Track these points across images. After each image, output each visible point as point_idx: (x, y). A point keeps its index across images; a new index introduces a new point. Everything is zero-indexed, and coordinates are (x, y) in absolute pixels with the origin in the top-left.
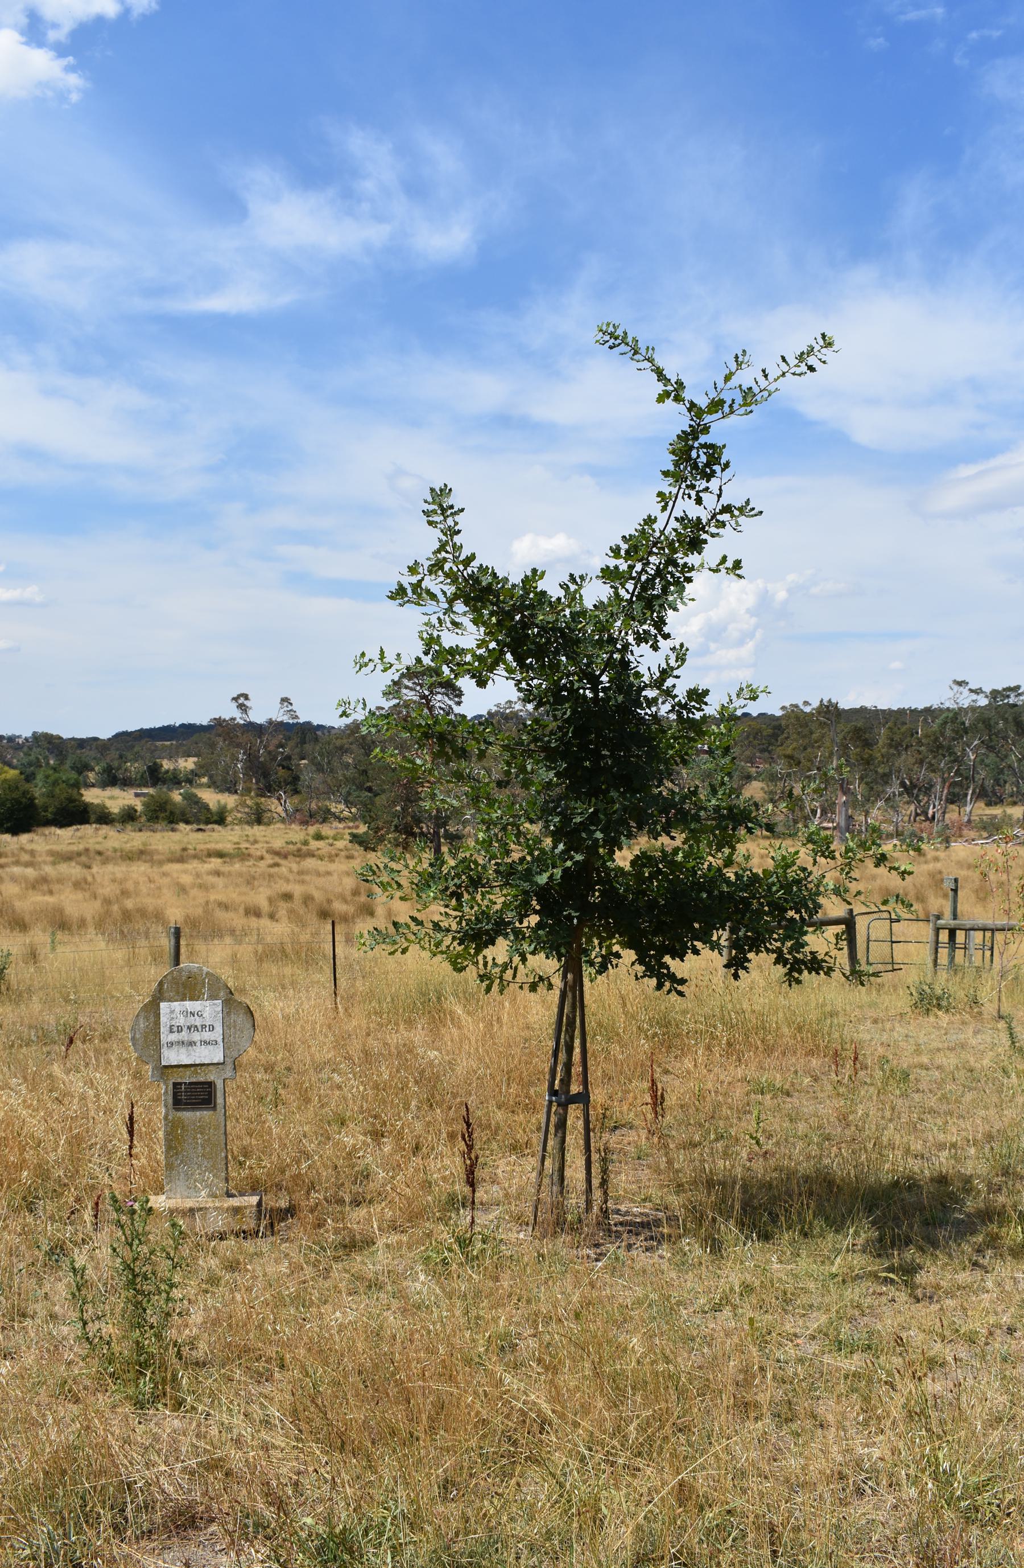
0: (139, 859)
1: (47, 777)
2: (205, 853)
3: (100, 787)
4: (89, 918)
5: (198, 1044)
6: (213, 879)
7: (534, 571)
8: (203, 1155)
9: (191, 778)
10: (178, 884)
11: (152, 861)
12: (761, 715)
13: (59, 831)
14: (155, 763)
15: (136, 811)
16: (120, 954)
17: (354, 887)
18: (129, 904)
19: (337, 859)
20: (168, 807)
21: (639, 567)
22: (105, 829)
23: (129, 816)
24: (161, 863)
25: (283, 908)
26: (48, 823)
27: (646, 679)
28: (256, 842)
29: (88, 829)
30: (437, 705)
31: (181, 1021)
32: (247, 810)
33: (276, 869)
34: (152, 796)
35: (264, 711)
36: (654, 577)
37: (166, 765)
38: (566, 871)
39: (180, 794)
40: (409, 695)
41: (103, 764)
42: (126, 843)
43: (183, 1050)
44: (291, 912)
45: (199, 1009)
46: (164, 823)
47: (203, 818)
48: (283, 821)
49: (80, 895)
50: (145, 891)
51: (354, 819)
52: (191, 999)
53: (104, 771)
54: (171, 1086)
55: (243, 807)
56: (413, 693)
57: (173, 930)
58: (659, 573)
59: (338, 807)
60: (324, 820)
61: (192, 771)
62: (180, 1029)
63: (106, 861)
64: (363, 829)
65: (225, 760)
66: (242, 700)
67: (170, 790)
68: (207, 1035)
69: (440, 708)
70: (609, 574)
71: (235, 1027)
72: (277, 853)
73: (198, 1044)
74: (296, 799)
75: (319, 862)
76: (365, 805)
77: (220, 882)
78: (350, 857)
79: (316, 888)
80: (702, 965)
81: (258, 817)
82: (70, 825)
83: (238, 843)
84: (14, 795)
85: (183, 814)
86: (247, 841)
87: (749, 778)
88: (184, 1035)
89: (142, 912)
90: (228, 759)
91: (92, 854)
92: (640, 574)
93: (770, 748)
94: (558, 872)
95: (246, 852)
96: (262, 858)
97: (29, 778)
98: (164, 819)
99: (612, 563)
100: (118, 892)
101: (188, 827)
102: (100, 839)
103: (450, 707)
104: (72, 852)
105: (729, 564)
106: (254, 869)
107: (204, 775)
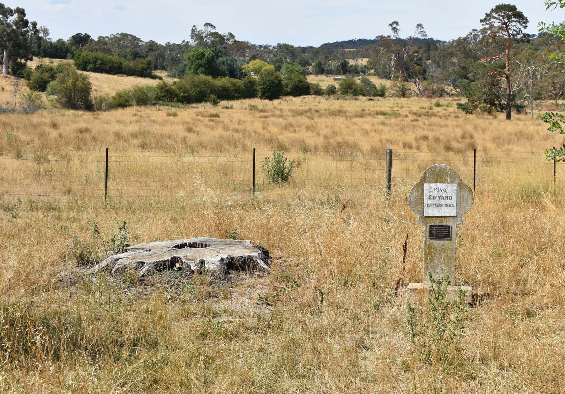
0: (338, 115)
1: (288, 68)
2: (375, 112)
5: (444, 206)
6: (381, 127)
8: (444, 264)
9: (364, 70)
10: (362, 129)
13: (294, 99)
14: (345, 61)
15: (335, 88)
16: (344, 165)
18: (339, 139)
19: (449, 118)
20: (353, 86)
22: (319, 98)
23: (332, 91)
24: (351, 117)
25: (424, 144)
26: (288, 94)
28: (402, 107)
29: (309, 98)
31: (435, 193)
32: (397, 89)
33: (415, 123)
34: (345, 80)
37: (351, 62)
39: (359, 79)
40: (497, 24)
42: (331, 106)
43: (436, 209)
44: (428, 146)
46: (351, 95)
48: (417, 95)
49: (310, 134)
50: (345, 132)
51: (458, 95)
52: (441, 182)
53: (317, 66)
54: (429, 227)
56: (498, 21)
57: (388, 151)
60: (441, 96)
61: (365, 66)
62: (434, 198)
63: (320, 116)
65: (384, 60)
66: (394, 25)
68: (448, 202)
69: (514, 30)
71: (463, 198)
72: (415, 114)
73: (444, 206)
74: (425, 83)
75: (439, 119)
76: (465, 87)
77: (386, 129)
78: (457, 117)
79: (440, 133)
81: (403, 93)
82: (300, 95)
83: (392, 108)
84: (272, 78)
85: (362, 90)
86: (398, 106)
88: (436, 201)
95: (398, 112)
96: (407, 116)
97: (278, 68)
100: (330, 132)
101: (364, 98)
102: (316, 104)
103: (520, 30)
104: (302, 110)
106: (404, 123)
107: (372, 69)
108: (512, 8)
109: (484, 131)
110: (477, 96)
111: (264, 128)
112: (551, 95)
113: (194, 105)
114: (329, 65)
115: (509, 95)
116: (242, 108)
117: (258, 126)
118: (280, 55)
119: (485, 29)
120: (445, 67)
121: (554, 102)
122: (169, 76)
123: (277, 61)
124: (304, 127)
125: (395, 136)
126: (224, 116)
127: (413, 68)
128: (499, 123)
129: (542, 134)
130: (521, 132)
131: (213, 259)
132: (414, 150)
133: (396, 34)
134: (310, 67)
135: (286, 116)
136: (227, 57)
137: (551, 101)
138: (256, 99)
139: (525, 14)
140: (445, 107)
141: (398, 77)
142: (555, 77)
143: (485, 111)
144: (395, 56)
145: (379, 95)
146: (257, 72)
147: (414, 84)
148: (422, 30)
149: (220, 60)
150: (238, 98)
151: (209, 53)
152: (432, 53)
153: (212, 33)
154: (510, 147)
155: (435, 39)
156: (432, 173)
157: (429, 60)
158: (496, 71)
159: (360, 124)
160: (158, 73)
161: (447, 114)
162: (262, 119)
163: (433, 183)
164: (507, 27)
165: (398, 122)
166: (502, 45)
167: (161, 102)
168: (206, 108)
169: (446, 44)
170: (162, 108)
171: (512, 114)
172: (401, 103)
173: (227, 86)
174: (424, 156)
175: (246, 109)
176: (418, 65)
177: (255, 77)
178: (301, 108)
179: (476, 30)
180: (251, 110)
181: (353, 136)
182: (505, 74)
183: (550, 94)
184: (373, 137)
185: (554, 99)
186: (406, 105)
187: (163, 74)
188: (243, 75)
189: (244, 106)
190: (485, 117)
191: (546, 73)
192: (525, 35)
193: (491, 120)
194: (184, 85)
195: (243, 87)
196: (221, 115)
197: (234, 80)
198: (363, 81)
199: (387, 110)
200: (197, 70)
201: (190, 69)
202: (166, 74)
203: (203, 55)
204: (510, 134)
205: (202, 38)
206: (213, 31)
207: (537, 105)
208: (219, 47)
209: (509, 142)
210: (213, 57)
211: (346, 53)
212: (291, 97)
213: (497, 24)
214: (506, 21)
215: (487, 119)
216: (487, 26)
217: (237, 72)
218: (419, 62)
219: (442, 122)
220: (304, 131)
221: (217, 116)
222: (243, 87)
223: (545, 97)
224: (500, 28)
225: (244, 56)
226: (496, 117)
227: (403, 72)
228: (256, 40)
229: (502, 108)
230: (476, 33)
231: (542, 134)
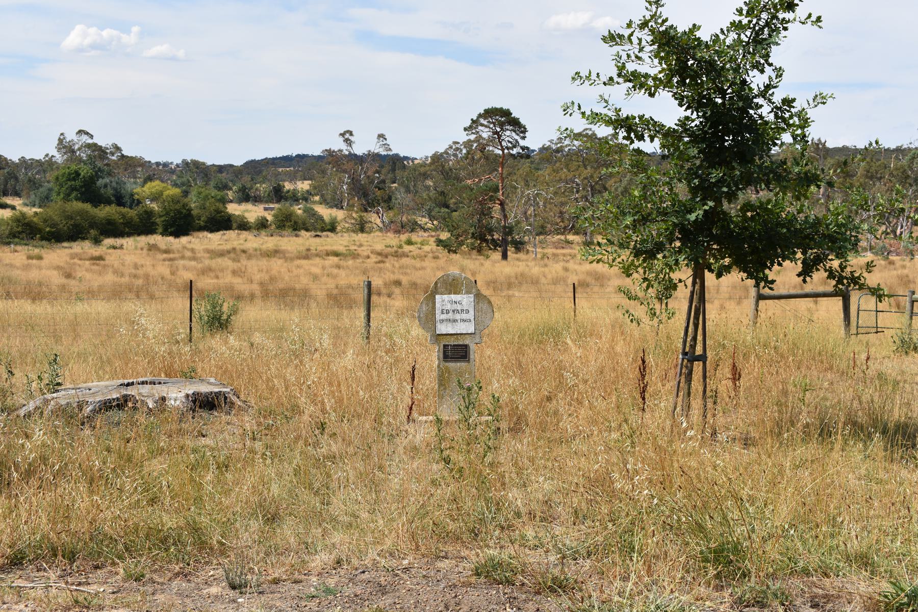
1: (200, 193)
6: (335, 271)
7: (694, 25)
10: (310, 273)
11: (286, 259)
13: (209, 235)
14: (279, 185)
21: (755, 21)
22: (245, 234)
23: (262, 225)
24: (292, 259)
25: (397, 291)
26: (201, 229)
27: (756, 92)
28: (361, 245)
29: (231, 234)
31: (449, 307)
32: (353, 221)
33: (381, 265)
36: (764, 27)
37: (288, 186)
38: (705, 211)
40: (486, 134)
42: (262, 244)
43: (450, 325)
48: (381, 230)
51: (436, 229)
52: (455, 293)
53: (240, 190)
54: (442, 347)
56: (487, 130)
58: (767, 24)
59: (423, 221)
61: (308, 191)
62: (448, 312)
63: (249, 257)
66: (347, 136)
68: (464, 316)
70: (737, 26)
72: (379, 254)
74: (391, 213)
75: (413, 261)
76: (444, 219)
77: (343, 273)
80: (786, 274)
81: (362, 227)
82: (218, 230)
84: (177, 207)
85: (304, 224)
92: (755, 25)
94: (701, 212)
96: (368, 257)
97: (186, 193)
99: (737, 19)
100: (267, 278)
101: (308, 234)
102: (242, 242)
103: (517, 141)
104: (223, 250)
105: (814, 18)
107: (316, 195)
108: (506, 113)
111: (173, 273)
113: (65, 244)
115: (505, 227)
116: (136, 248)
117: (163, 269)
118: (187, 177)
119: (469, 141)
120: (417, 192)
121: (563, 237)
122: (26, 205)
123: (183, 184)
124: (229, 272)
126: (112, 258)
128: (491, 267)
129: (549, 276)
130: (522, 275)
131: (177, 394)
133: (349, 148)
134: (230, 193)
135: (200, 258)
136: (110, 178)
137: (559, 237)
138: (155, 236)
139: (522, 121)
140: (419, 246)
141: (353, 206)
143: (473, 249)
144: (349, 178)
145: (329, 230)
146: (155, 198)
148: (385, 142)
149: (100, 182)
150: (129, 235)
151: (85, 171)
152: (399, 173)
153: (89, 144)
154: (511, 292)
155: (402, 156)
159: (307, 268)
160: (9, 200)
161: (423, 254)
162: (167, 263)
164: (499, 138)
166: (493, 163)
167: (17, 240)
168: (84, 247)
169: (416, 162)
170: (19, 248)
171: (509, 253)
173: (113, 217)
175: (142, 249)
176: (379, 189)
177: (155, 206)
178: (221, 247)
180: (149, 250)
182: (499, 200)
185: (562, 234)
187: (17, 202)
188: (135, 202)
189: (139, 246)
191: (551, 198)
192: (523, 148)
194: (50, 217)
195: (136, 219)
196: (107, 257)
197: (125, 210)
198: (306, 210)
199: (341, 249)
200: (69, 195)
201: (59, 194)
202: (21, 202)
203: (77, 174)
205: (73, 152)
206: (90, 141)
207: (540, 242)
208: (99, 164)
210: (91, 178)
211: (279, 174)
212: (205, 233)
213: (486, 134)
214: (498, 129)
216: (473, 137)
217: (127, 199)
218: (381, 186)
219: (418, 264)
220: (230, 276)
221: (100, 258)
222: (136, 219)
224: (490, 141)
225: (135, 178)
228: (152, 157)
229: (495, 244)
231: (549, 276)
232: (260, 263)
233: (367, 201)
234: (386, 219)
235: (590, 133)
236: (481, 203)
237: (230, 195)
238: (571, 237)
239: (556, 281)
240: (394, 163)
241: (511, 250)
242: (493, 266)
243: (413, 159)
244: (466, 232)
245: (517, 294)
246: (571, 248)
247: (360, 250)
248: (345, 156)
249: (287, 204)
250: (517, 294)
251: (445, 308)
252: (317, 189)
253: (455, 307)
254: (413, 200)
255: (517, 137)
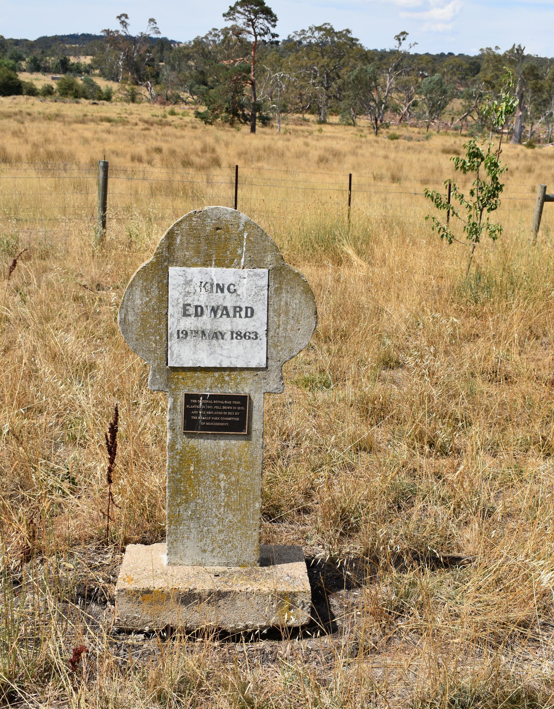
2: (99, 118)
3: (29, 72)
4: (23, 155)
5: (228, 336)
6: (105, 136)
8: (227, 505)
9: (88, 70)
10: (83, 137)
11: (64, 122)
12: (461, 55)
14: (65, 58)
15: (53, 88)
16: (48, 182)
17: (202, 146)
18: (52, 148)
19: (186, 129)
20: (74, 87)
22: (33, 99)
23: (48, 92)
24: (70, 123)
25: (157, 158)
28: (131, 114)
29: (21, 99)
30: (259, 26)
31: (202, 298)
32: (125, 92)
33: (146, 132)
34: (64, 79)
35: (135, 29)
37: (73, 60)
39: (82, 80)
41: (32, 57)
43: (203, 344)
44: (162, 160)
45: (231, 280)
46: (72, 97)
47: (96, 96)
48: (149, 101)
49: (16, 140)
51: (195, 103)
52: (220, 264)
53: (32, 61)
54: (181, 399)
55: (123, 90)
56: (243, 17)
57: (102, 164)
59: (185, 95)
60: (176, 103)
61: (89, 65)
62: (199, 312)
63: (33, 120)
64: (203, 109)
67: (75, 76)
68: (242, 324)
69: (261, 29)
71: (287, 313)
72: (146, 122)
73: (228, 336)
74: (158, 87)
75: (175, 130)
76: (203, 95)
77: (111, 137)
78: (194, 128)
79: (177, 144)
81: (133, 98)
82: (9, 94)
83: (120, 114)
85: (84, 92)
87: (453, 96)
88: (206, 322)
89: (61, 154)
90: (113, 58)
91: (24, 115)
93: (466, 77)
95: (126, 119)
96: (136, 124)
98: (71, 95)
100: (42, 140)
101: (87, 101)
102: (29, 106)
103: (268, 29)
104: (11, 113)
106: (133, 131)
107: (97, 68)
109: (227, 145)
110: (218, 104)
112: (297, 108)
114: (46, 61)
115: (254, 104)
119: (226, 28)
121: (301, 116)
125: (121, 147)
127: (144, 70)
128: (242, 138)
129: (293, 150)
132: (145, 165)
133: (125, 29)
137: (298, 115)
139: (274, 11)
140: (181, 116)
141: (127, 79)
142: (302, 87)
143: (226, 122)
145: (105, 99)
147: (145, 88)
148: (155, 26)
154: (260, 164)
155: (170, 39)
156: (194, 233)
157: (162, 62)
158: (240, 75)
161: (183, 124)
163: (195, 265)
165: (126, 131)
166: (245, 47)
169: (181, 45)
171: (257, 127)
172: (130, 109)
174: (158, 173)
176: (149, 66)
179: (217, 30)
181: (70, 145)
182: (250, 80)
183: (296, 107)
184: (94, 147)
185: (301, 113)
186: (136, 112)
190: (227, 129)
193: (234, 133)
198: (86, 81)
199: (114, 116)
204: (257, 150)
209: (259, 159)
214: (253, 17)
215: (229, 131)
219: (178, 132)
223: (291, 109)
226: (239, 130)
227: (132, 74)
229: (246, 119)
230: (217, 32)
231: (293, 150)
232: (41, 125)
233: (139, 76)
234: (154, 93)
235: (328, 27)
236: (235, 82)
237: (24, 64)
238: (307, 116)
239: (299, 155)
240: (162, 44)
241: (258, 123)
242: (243, 137)
243: (179, 43)
244: (220, 106)
245: (266, 166)
246: (308, 125)
247: (130, 118)
248: (121, 36)
249: (71, 75)
250: (266, 166)
251: (194, 300)
252: (96, 64)
253: (218, 299)
254: (177, 77)
255: (269, 25)
